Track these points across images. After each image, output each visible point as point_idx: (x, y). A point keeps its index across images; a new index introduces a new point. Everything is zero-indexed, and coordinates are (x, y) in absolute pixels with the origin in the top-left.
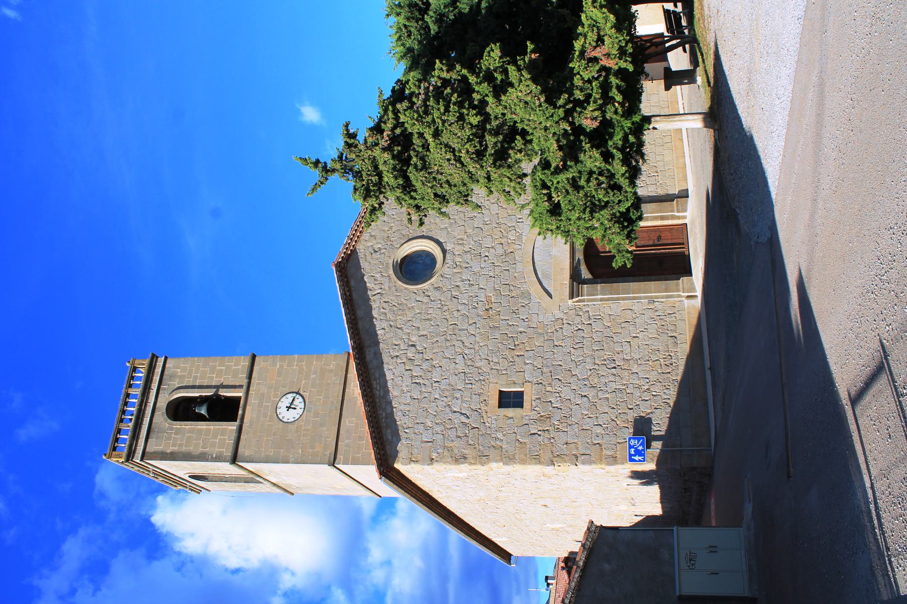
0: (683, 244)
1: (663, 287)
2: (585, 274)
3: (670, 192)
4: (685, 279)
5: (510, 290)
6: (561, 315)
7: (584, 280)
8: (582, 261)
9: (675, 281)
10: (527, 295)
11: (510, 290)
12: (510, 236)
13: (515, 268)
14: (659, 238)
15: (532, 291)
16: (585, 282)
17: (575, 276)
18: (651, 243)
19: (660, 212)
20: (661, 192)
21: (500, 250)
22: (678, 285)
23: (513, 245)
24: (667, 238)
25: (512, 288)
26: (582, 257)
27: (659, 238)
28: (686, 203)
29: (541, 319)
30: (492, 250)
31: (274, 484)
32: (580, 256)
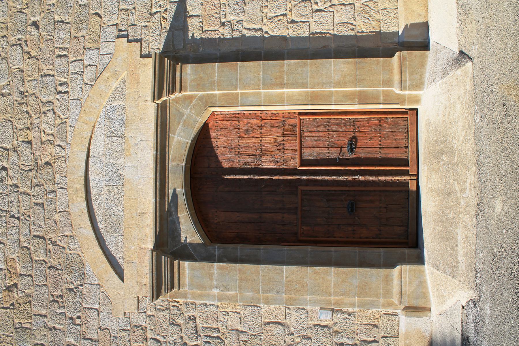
0: (406, 163)
1: (356, 282)
2: (189, 233)
3: (386, 29)
4: (404, 271)
5: (48, 252)
6: (141, 320)
7: (186, 246)
8: (182, 200)
9: (383, 271)
10: (76, 266)
11: (48, 252)
12: (44, 126)
13: (53, 202)
14: (353, 143)
15: (86, 258)
16: (185, 253)
17: (167, 246)
18: (334, 155)
19: (360, 82)
20: (363, 26)
21: (27, 159)
22: (388, 280)
23: (50, 149)
24: (370, 146)
25: (50, 247)
26: (181, 191)
27: (353, 143)
28: (423, 64)
29: (104, 322)
30: (13, 157)
31: (91, 137)
32: (177, 183)
